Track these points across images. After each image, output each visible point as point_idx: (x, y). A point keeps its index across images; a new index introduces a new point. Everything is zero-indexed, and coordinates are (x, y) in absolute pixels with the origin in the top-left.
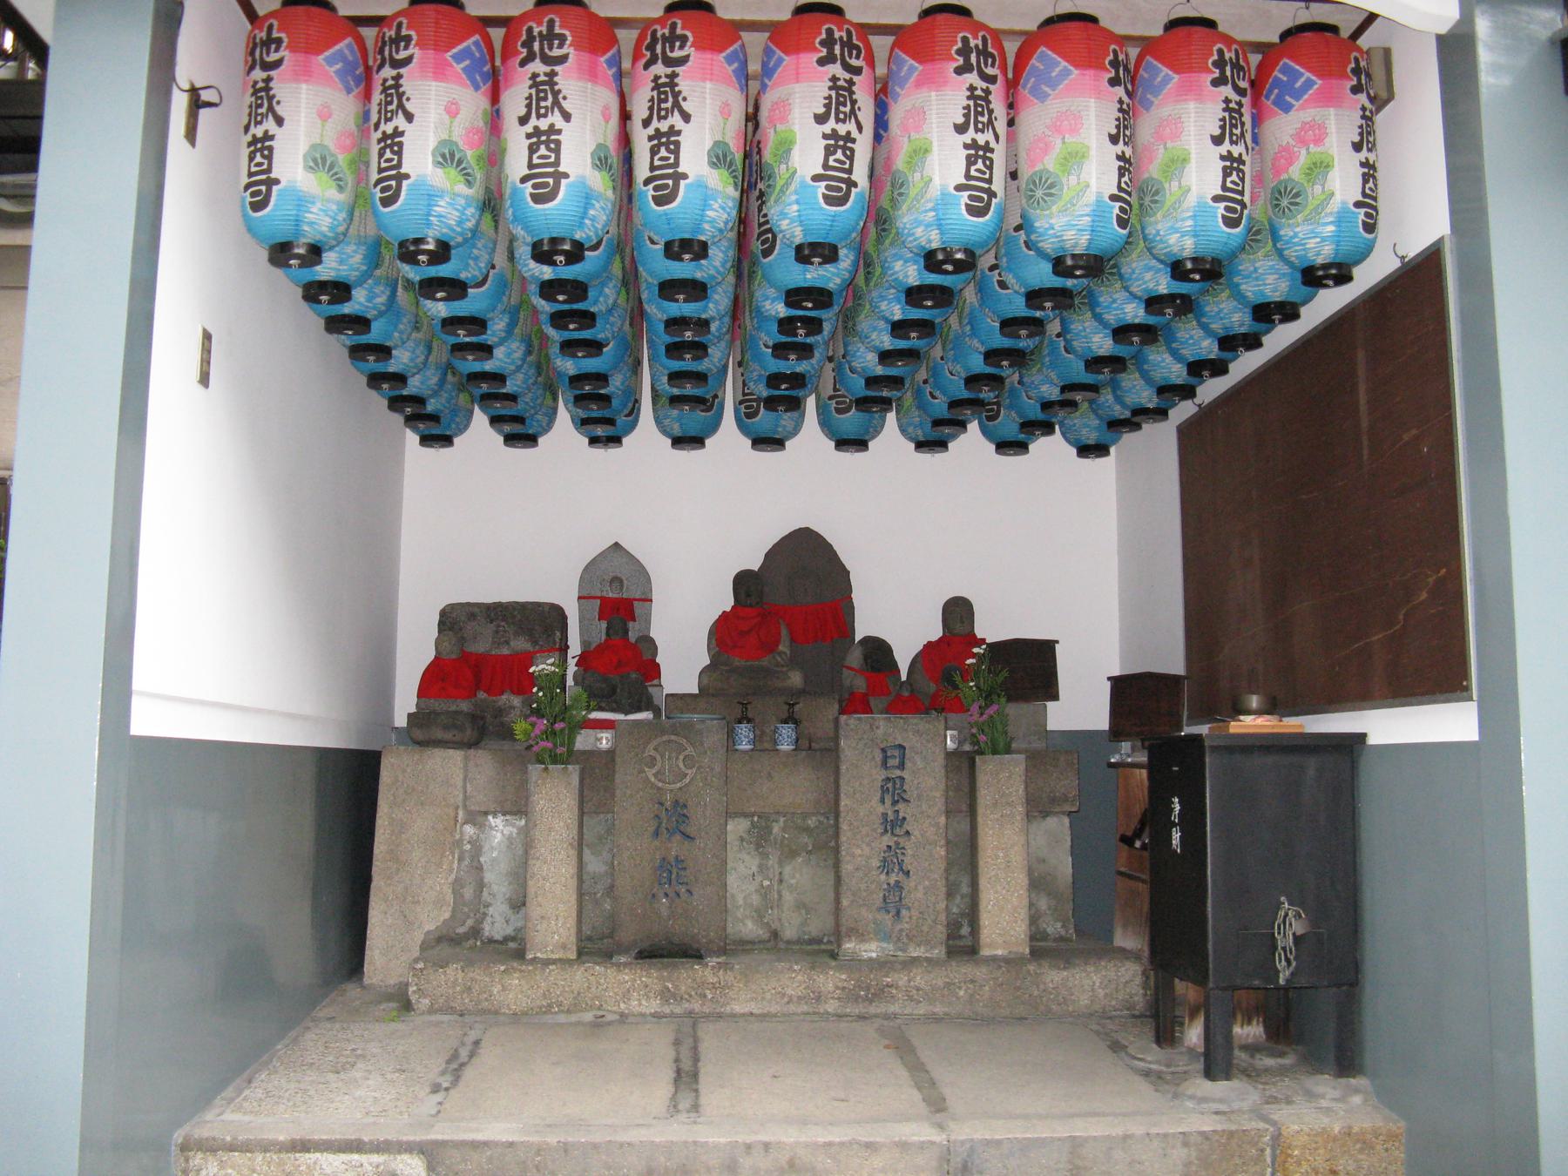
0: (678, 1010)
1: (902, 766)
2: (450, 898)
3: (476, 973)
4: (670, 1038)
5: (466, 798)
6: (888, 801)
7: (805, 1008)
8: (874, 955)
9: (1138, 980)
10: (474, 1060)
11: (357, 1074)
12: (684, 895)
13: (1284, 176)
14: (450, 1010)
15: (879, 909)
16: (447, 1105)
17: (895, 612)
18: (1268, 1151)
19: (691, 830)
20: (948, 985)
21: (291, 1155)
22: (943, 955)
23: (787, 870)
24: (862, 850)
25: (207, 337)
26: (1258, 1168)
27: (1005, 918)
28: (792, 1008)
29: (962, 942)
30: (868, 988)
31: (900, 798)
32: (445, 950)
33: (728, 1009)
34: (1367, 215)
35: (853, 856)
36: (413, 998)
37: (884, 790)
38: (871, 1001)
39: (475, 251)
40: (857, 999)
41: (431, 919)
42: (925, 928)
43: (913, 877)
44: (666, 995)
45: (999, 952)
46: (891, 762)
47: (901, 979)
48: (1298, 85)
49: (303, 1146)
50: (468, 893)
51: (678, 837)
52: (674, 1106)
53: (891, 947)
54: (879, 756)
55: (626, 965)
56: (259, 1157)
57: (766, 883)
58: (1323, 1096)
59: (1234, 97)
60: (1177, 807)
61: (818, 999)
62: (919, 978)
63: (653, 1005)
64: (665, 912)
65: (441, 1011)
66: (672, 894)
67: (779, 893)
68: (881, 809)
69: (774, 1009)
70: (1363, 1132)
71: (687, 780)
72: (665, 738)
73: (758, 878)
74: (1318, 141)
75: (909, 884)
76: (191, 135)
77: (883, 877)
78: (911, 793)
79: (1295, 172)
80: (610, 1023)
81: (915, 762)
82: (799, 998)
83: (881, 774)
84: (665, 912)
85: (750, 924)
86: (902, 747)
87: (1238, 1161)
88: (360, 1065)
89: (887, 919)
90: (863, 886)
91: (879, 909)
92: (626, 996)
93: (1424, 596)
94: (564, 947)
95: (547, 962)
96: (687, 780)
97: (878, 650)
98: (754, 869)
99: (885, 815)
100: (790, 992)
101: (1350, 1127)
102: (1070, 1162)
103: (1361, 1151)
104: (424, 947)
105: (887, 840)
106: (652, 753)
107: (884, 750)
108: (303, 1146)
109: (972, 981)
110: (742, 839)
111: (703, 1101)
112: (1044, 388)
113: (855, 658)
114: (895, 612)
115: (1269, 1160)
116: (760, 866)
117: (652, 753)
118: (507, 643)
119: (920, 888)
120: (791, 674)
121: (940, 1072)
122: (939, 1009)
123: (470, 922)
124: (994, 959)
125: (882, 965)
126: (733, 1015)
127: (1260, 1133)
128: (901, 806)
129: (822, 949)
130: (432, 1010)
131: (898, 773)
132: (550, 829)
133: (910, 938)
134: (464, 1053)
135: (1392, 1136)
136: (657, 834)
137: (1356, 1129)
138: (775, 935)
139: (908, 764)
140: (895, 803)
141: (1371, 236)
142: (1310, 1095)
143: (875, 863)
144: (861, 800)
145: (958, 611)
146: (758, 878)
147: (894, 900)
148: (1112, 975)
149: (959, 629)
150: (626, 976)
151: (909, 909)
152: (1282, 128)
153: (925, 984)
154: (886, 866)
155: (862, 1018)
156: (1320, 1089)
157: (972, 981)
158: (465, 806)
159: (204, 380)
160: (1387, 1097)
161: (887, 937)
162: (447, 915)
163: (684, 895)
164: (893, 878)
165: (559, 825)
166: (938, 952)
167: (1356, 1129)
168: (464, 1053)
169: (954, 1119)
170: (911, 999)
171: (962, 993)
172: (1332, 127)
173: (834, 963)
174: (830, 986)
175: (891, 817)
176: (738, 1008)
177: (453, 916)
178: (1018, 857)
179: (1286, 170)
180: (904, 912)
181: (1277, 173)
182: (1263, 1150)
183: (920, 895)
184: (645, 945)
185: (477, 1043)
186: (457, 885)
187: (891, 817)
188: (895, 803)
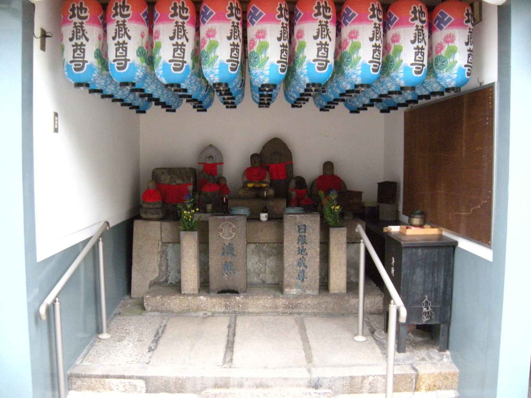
0: (231, 311)
1: (305, 232)
2: (158, 270)
3: (165, 299)
4: (227, 324)
5: (161, 238)
6: (300, 244)
7: (272, 310)
8: (295, 293)
9: (382, 301)
10: (164, 335)
11: (125, 342)
12: (232, 274)
13: (439, 54)
14: (158, 311)
15: (297, 278)
16: (153, 358)
17: (307, 164)
18: (414, 380)
19: (235, 253)
20: (318, 303)
21: (103, 379)
22: (318, 293)
23: (268, 261)
24: (290, 259)
25: (56, 115)
26: (411, 385)
27: (338, 279)
28: (268, 310)
29: (324, 285)
30: (292, 304)
31: (304, 242)
32: (156, 288)
33: (247, 311)
34: (469, 70)
35: (288, 261)
36: (146, 307)
37: (299, 240)
38: (294, 308)
39: (147, 80)
40: (289, 307)
41: (154, 276)
42: (312, 285)
43: (308, 268)
44: (226, 306)
45: (336, 292)
46: (301, 231)
47: (304, 301)
48: (445, 20)
49: (107, 377)
50: (164, 268)
51: (230, 255)
52: (224, 362)
53: (300, 290)
54: (297, 228)
55: (214, 296)
56: (93, 380)
57: (261, 265)
58: (434, 359)
59: (420, 24)
60: (394, 261)
61: (276, 308)
62: (309, 301)
63: (223, 309)
64: (226, 280)
65: (154, 311)
66: (228, 273)
67: (265, 268)
68: (297, 246)
69: (262, 310)
70: (445, 373)
71: (233, 236)
72: (226, 222)
73: (258, 264)
74: (452, 41)
75: (307, 270)
76: (43, 48)
77: (298, 268)
78: (308, 241)
79: (443, 53)
80: (209, 316)
81: (309, 230)
82: (270, 307)
83: (298, 234)
84: (226, 280)
85: (255, 279)
86: (305, 225)
87: (404, 383)
88: (127, 338)
89: (299, 282)
90: (291, 271)
91: (297, 278)
92: (214, 306)
93: (479, 207)
94: (194, 290)
95: (189, 295)
96: (233, 236)
97: (301, 181)
98: (257, 260)
99: (299, 248)
100: (267, 305)
101: (441, 372)
102: (350, 383)
103: (444, 379)
104: (150, 286)
105: (300, 256)
106: (221, 227)
107: (299, 226)
108: (107, 377)
109: (327, 302)
110: (253, 251)
111: (234, 357)
112: (357, 103)
113: (293, 184)
114: (307, 164)
115: (414, 382)
116: (259, 260)
117: (221, 227)
118: (175, 182)
119: (311, 272)
120: (269, 190)
121: (313, 343)
122: (316, 311)
123: (164, 278)
124: (334, 294)
125: (297, 297)
126: (249, 313)
127: (412, 375)
128: (304, 245)
129: (278, 287)
130: (152, 311)
131: (304, 234)
132: (188, 252)
133: (307, 288)
134: (160, 331)
135: (454, 375)
136: (223, 254)
137: (443, 373)
138: (264, 282)
139: (307, 231)
140: (302, 244)
141: (469, 77)
142: (431, 358)
143: (296, 263)
144: (291, 245)
145: (328, 166)
146: (258, 264)
147: (302, 276)
148: (373, 300)
149: (328, 173)
150: (214, 300)
151: (306, 278)
152: (439, 36)
153: (313, 300)
154: (299, 264)
155: (291, 314)
156: (433, 356)
157: (327, 302)
158: (161, 241)
159: (56, 130)
160: (455, 360)
161: (299, 287)
162: (157, 275)
163: (232, 274)
164: (301, 268)
165: (191, 251)
166: (316, 292)
167: (443, 373)
168: (160, 331)
169: (314, 367)
170: (306, 308)
171: (323, 306)
172: (457, 38)
173: (281, 296)
174: (280, 303)
175: (301, 248)
176: (250, 310)
177: (159, 277)
178: (344, 262)
179: (440, 52)
180: (305, 279)
181: (437, 53)
182: (412, 380)
183: (310, 274)
184: (220, 290)
185: (165, 326)
186: (160, 265)
187: (301, 248)
188: (302, 244)
